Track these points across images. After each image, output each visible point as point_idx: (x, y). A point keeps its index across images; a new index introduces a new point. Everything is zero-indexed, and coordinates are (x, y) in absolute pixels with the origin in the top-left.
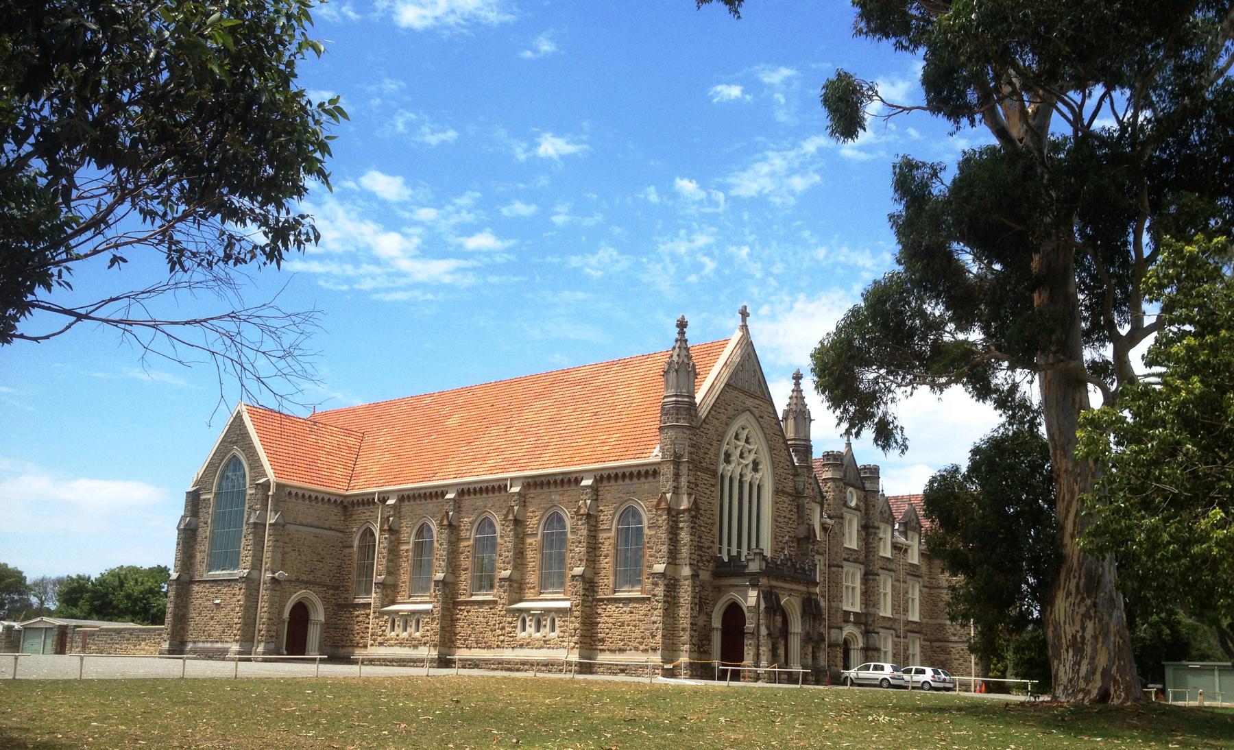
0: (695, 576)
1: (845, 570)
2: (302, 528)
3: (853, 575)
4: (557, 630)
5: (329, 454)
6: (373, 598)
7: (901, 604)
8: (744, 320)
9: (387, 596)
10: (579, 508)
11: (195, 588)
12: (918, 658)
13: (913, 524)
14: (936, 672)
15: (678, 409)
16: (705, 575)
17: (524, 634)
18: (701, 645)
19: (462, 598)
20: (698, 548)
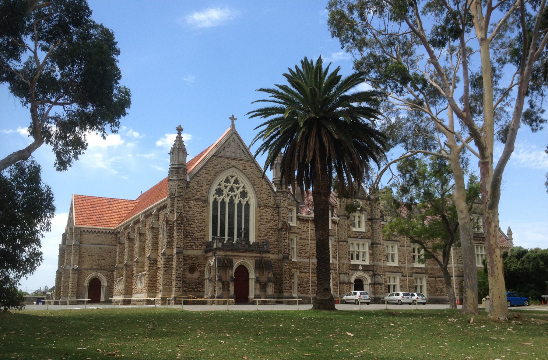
3: (363, 245)
5: (114, 212)
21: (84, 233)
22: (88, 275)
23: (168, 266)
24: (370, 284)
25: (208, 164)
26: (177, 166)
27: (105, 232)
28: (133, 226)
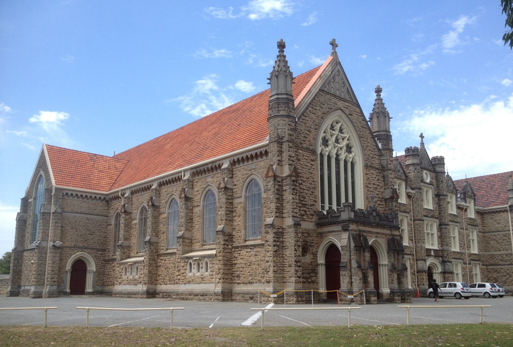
0: (297, 225)
1: (426, 223)
2: (78, 215)
3: (431, 226)
4: (209, 270)
5: (100, 171)
6: (118, 255)
7: (465, 243)
8: (334, 48)
9: (124, 253)
10: (220, 184)
11: (25, 254)
12: (479, 277)
13: (470, 193)
14: (493, 286)
15: (279, 104)
16: (308, 225)
17: (191, 274)
18: (307, 275)
19: (162, 252)
20: (302, 204)
21: (66, 197)
22: (71, 255)
23: (278, 243)
24: (441, 273)
25: (315, 101)
26: (285, 96)
27: (95, 198)
28: (158, 188)
